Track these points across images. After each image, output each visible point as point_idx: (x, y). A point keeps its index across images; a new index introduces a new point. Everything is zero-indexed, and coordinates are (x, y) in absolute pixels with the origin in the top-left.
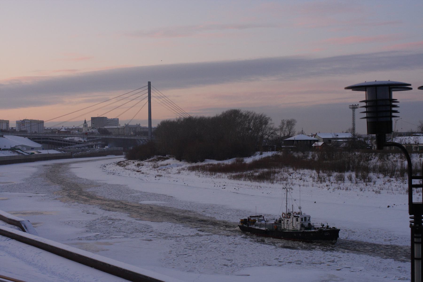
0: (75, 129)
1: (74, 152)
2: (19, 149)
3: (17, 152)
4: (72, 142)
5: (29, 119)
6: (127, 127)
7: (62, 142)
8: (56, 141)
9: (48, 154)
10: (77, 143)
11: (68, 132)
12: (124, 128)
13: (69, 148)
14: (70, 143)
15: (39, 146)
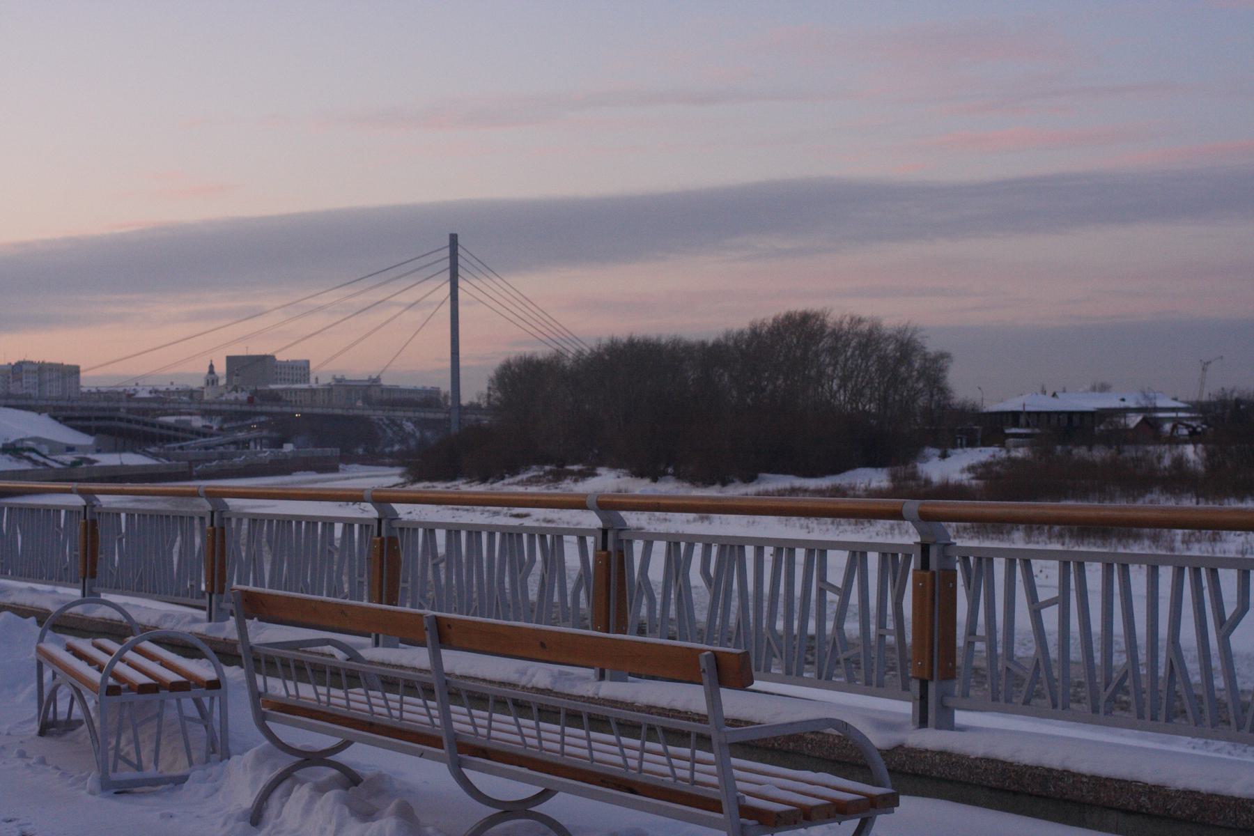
0: (178, 392)
1: (198, 461)
2: (33, 450)
3: (29, 459)
4: (184, 430)
6: (341, 386)
8: (138, 427)
9: (122, 466)
10: (199, 433)
11: (163, 400)
12: (329, 389)
13: (181, 448)
14: (180, 434)
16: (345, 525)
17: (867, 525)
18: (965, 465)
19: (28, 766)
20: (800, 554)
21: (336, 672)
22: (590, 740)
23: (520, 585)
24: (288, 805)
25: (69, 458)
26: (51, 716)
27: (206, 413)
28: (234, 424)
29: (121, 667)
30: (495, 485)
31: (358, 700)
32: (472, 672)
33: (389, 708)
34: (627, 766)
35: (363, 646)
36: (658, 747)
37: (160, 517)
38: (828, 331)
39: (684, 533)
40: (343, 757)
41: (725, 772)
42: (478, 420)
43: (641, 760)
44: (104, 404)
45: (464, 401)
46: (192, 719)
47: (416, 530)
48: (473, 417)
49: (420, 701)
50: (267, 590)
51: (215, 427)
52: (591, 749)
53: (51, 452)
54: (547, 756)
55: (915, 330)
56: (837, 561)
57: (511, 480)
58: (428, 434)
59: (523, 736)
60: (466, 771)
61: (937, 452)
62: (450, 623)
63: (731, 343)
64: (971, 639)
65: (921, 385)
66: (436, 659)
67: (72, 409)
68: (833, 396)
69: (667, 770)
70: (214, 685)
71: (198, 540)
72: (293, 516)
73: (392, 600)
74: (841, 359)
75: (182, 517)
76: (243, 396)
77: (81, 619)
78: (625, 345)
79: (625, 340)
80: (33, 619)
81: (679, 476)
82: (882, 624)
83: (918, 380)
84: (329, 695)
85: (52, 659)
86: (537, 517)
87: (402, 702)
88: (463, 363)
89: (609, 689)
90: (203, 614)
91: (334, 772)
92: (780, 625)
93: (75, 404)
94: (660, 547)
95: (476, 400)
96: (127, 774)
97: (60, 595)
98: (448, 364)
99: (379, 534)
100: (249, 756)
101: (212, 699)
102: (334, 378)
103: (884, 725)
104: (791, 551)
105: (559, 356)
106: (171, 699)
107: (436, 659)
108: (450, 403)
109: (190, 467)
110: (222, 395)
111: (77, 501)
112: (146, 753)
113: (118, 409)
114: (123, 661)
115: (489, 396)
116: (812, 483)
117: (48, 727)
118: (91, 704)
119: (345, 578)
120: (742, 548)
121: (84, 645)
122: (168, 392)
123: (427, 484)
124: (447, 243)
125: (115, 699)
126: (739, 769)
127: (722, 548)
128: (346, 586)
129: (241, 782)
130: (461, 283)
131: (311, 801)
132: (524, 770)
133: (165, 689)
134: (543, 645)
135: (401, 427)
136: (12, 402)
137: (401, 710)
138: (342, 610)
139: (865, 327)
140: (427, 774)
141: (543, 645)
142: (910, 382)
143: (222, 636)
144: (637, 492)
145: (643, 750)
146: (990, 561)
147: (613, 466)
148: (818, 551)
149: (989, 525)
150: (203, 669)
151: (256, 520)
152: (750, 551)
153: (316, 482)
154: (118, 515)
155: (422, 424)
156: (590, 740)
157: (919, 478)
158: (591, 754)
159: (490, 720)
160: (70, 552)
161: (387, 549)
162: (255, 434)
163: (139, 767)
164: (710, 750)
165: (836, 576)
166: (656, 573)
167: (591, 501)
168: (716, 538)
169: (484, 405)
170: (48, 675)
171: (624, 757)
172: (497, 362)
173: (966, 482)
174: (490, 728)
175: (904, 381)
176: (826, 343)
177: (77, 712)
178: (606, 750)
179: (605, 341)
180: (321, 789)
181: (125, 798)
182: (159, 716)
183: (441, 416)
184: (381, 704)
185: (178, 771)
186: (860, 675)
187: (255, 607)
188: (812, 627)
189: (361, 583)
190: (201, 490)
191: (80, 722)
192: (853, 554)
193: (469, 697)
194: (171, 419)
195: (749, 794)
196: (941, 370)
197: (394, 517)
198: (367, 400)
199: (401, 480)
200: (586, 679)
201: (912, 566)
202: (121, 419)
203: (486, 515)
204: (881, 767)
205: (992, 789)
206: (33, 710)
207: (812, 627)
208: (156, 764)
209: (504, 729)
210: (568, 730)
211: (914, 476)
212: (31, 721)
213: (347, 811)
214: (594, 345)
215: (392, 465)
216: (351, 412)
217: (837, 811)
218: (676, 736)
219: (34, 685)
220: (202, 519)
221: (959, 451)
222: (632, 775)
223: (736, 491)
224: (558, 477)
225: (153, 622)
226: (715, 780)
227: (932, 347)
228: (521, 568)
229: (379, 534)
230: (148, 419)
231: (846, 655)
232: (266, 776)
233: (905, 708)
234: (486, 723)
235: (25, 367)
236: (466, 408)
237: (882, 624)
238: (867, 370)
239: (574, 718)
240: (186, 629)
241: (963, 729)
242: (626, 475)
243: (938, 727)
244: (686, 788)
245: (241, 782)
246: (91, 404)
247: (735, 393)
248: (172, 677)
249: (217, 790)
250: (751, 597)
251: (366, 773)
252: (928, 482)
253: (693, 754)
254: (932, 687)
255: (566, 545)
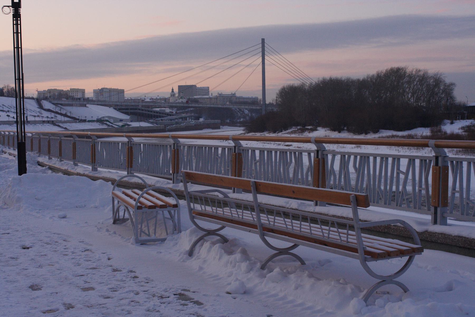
0: (161, 99)
2: (107, 121)
3: (106, 124)
4: (163, 113)
5: (108, 87)
6: (221, 97)
7: (152, 113)
10: (168, 114)
11: (155, 102)
12: (216, 98)
13: (162, 120)
14: (161, 115)
15: (127, 117)
16: (222, 148)
17: (421, 149)
18: (460, 126)
19: (110, 234)
20: (390, 160)
21: (219, 202)
22: (310, 227)
23: (286, 170)
24: (202, 249)
25: (120, 124)
26: (117, 217)
27: (171, 107)
28: (181, 111)
29: (142, 199)
30: (279, 134)
31: (227, 212)
32: (269, 203)
33: (238, 215)
34: (324, 236)
35: (229, 193)
36: (335, 229)
37: (156, 145)
38: (407, 75)
39: (347, 152)
40: (221, 232)
41: (359, 238)
42: (272, 109)
43: (329, 234)
44: (133, 104)
45: (267, 102)
46: (168, 218)
47: (248, 150)
48: (271, 108)
49: (249, 212)
50: (194, 172)
51: (174, 112)
52: (311, 230)
53: (115, 122)
54: (295, 232)
55: (441, 75)
56: (404, 163)
57: (285, 132)
58: (254, 115)
59: (286, 225)
60: (266, 238)
61: (449, 121)
62: (260, 184)
63: (369, 80)
64: (454, 192)
65: (443, 96)
66: (255, 198)
67: (121, 106)
68: (409, 100)
69: (338, 238)
70: (176, 206)
71: (169, 154)
72: (204, 145)
73: (240, 175)
74: (412, 86)
75: (163, 146)
76: (184, 101)
77: (128, 183)
78: (328, 81)
79: (328, 79)
80: (110, 182)
81: (349, 131)
82: (420, 186)
83: (442, 94)
84: (217, 210)
85: (118, 197)
86: (295, 145)
87: (243, 213)
88: (267, 87)
89: (319, 209)
90: (171, 182)
91: (218, 238)
92: (382, 188)
93: (123, 104)
94: (338, 158)
95: (271, 102)
96: (144, 237)
97: (119, 174)
98: (261, 88)
99: (235, 152)
100: (188, 231)
101: (175, 211)
102: (218, 93)
103: (420, 223)
104: (387, 159)
105: (303, 85)
106: (160, 211)
107: (255, 198)
108: (262, 103)
109: (165, 127)
110: (177, 100)
111: (125, 140)
112: (151, 231)
113: (138, 106)
114: (143, 197)
115: (277, 100)
116: (400, 133)
117: (116, 221)
118: (132, 213)
119: (222, 169)
120: (368, 157)
121: (129, 192)
122: (157, 99)
123: (253, 133)
124: (261, 42)
125: (140, 211)
126: (365, 238)
127: (361, 157)
128: (223, 172)
129: (185, 240)
130: (266, 57)
131: (211, 247)
132: (287, 237)
133: (158, 207)
134: (294, 192)
135: (243, 112)
136: (100, 103)
137: (243, 215)
138: (221, 179)
139: (421, 73)
140: (252, 239)
141: (294, 192)
142: (439, 95)
143: (178, 189)
144: (333, 137)
145: (329, 230)
146: (461, 162)
147: (324, 127)
148: (396, 159)
149: (469, 149)
150: (171, 201)
151: (190, 147)
152: (371, 159)
153: (212, 132)
154: (140, 145)
155: (251, 111)
156: (310, 227)
157: (442, 132)
158: (323, 234)
159: (275, 219)
160: (123, 158)
161: (238, 157)
162: (189, 115)
163: (149, 235)
164: (354, 231)
165: (403, 168)
166: (337, 167)
167: (313, 140)
168: (359, 154)
169: (275, 104)
170: (116, 202)
171: (323, 233)
172: (280, 87)
173: (460, 133)
174: (274, 222)
175: (437, 94)
176: (406, 79)
177: (127, 216)
178: (316, 230)
179: (321, 79)
180: (214, 243)
181: (144, 246)
182: (156, 217)
183: (258, 108)
184: (235, 213)
185: (163, 237)
186: (412, 205)
187: (190, 178)
188: (394, 188)
189: (228, 170)
190: (170, 135)
191: (128, 219)
192: (410, 160)
193: (267, 211)
194: (158, 109)
195: (368, 247)
196: (452, 90)
197: (240, 146)
198: (231, 102)
199: (244, 132)
200: (310, 205)
201: (432, 165)
202: (139, 109)
203: (275, 145)
204: (417, 238)
205: (460, 247)
206: (111, 215)
207: (394, 188)
208: (155, 234)
209: (280, 222)
210: (303, 223)
211: (440, 131)
212: (109, 219)
213: (223, 251)
214: (316, 81)
215: (240, 126)
216: (225, 106)
217: (401, 253)
218: (342, 226)
219: (111, 206)
220: (170, 146)
221: (458, 121)
222: (326, 239)
223: (371, 136)
224: (303, 131)
225: (153, 184)
226: (355, 241)
227: (448, 81)
228: (287, 165)
229: (235, 152)
230: (150, 109)
231: (407, 197)
232: (194, 239)
233: (429, 218)
234: (273, 220)
235: (104, 90)
236: (268, 105)
237: (420, 186)
238: (422, 90)
239: (305, 219)
240: (165, 186)
241: (450, 225)
242: (328, 130)
243: (441, 224)
244: (345, 244)
245: (185, 240)
246: (129, 104)
247: (371, 99)
248: (160, 203)
249: (177, 244)
250: (372, 176)
251: (230, 238)
252: (445, 133)
253: (348, 232)
254: (439, 209)
255: (303, 156)
